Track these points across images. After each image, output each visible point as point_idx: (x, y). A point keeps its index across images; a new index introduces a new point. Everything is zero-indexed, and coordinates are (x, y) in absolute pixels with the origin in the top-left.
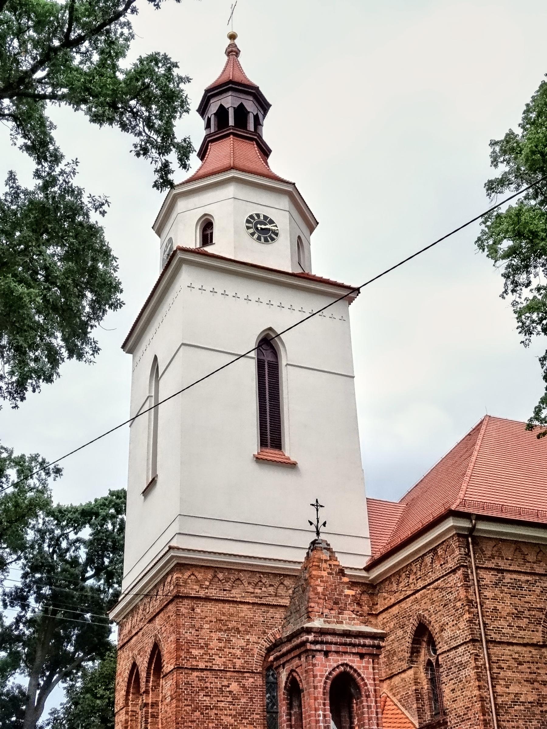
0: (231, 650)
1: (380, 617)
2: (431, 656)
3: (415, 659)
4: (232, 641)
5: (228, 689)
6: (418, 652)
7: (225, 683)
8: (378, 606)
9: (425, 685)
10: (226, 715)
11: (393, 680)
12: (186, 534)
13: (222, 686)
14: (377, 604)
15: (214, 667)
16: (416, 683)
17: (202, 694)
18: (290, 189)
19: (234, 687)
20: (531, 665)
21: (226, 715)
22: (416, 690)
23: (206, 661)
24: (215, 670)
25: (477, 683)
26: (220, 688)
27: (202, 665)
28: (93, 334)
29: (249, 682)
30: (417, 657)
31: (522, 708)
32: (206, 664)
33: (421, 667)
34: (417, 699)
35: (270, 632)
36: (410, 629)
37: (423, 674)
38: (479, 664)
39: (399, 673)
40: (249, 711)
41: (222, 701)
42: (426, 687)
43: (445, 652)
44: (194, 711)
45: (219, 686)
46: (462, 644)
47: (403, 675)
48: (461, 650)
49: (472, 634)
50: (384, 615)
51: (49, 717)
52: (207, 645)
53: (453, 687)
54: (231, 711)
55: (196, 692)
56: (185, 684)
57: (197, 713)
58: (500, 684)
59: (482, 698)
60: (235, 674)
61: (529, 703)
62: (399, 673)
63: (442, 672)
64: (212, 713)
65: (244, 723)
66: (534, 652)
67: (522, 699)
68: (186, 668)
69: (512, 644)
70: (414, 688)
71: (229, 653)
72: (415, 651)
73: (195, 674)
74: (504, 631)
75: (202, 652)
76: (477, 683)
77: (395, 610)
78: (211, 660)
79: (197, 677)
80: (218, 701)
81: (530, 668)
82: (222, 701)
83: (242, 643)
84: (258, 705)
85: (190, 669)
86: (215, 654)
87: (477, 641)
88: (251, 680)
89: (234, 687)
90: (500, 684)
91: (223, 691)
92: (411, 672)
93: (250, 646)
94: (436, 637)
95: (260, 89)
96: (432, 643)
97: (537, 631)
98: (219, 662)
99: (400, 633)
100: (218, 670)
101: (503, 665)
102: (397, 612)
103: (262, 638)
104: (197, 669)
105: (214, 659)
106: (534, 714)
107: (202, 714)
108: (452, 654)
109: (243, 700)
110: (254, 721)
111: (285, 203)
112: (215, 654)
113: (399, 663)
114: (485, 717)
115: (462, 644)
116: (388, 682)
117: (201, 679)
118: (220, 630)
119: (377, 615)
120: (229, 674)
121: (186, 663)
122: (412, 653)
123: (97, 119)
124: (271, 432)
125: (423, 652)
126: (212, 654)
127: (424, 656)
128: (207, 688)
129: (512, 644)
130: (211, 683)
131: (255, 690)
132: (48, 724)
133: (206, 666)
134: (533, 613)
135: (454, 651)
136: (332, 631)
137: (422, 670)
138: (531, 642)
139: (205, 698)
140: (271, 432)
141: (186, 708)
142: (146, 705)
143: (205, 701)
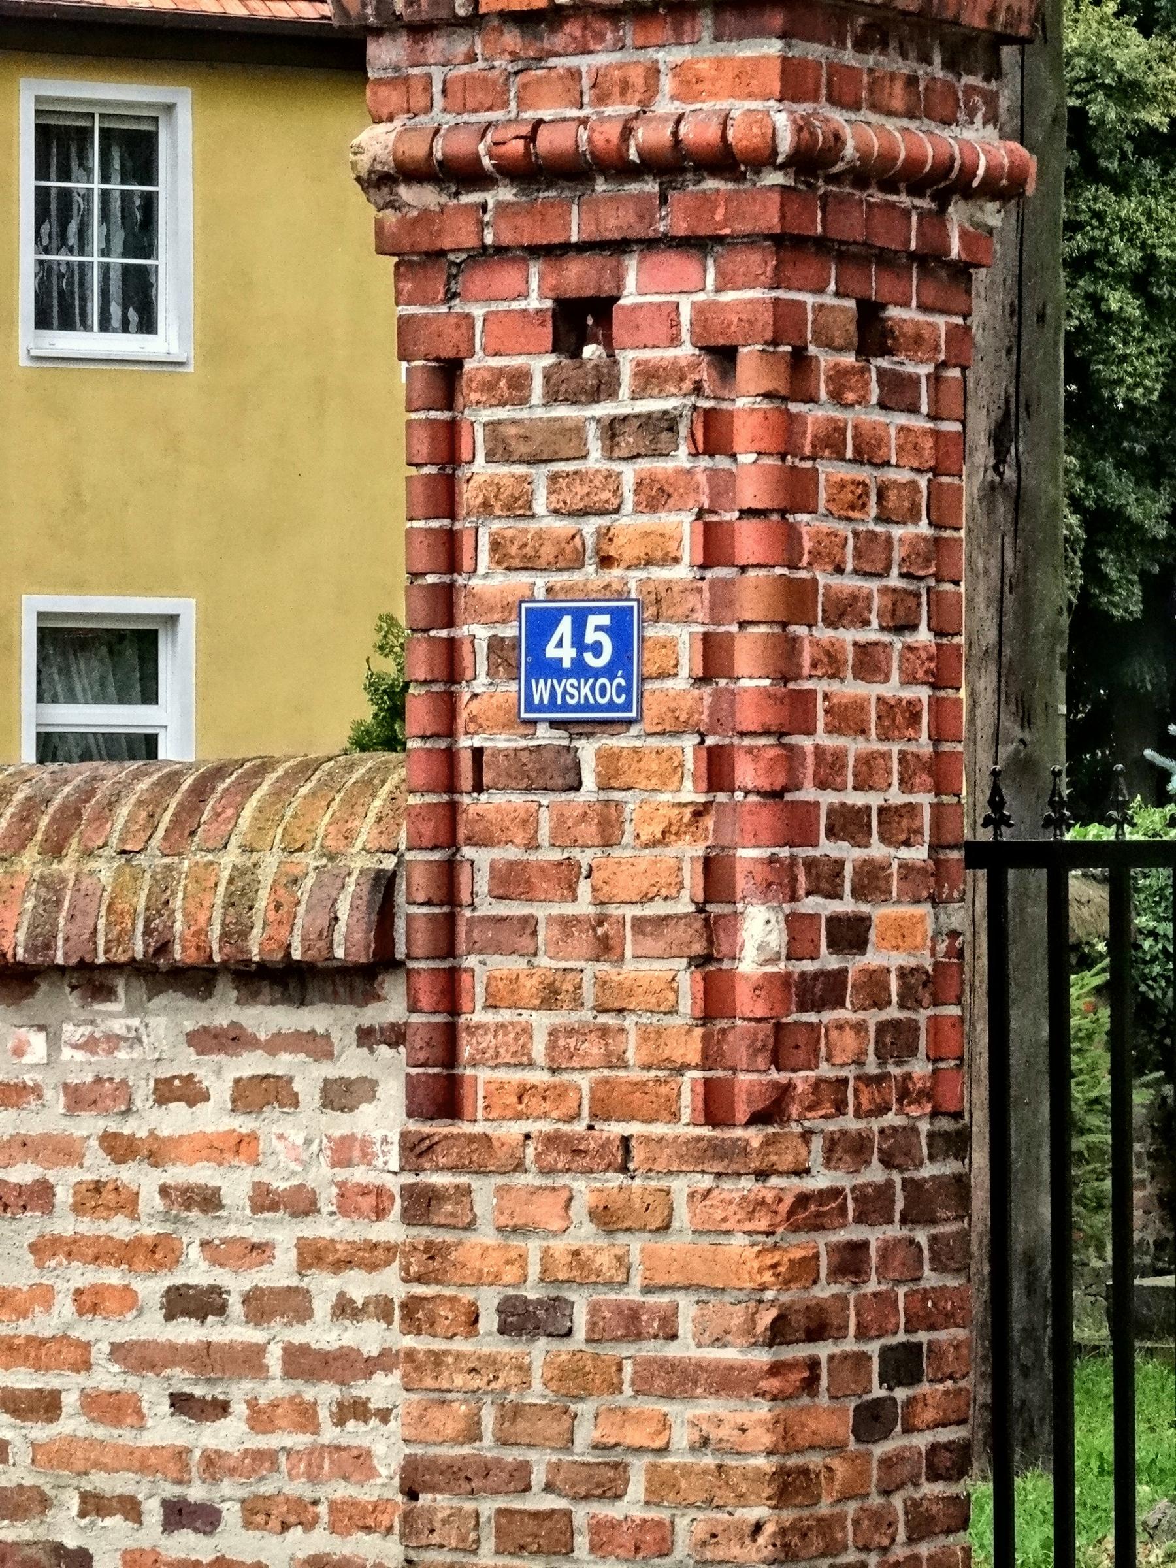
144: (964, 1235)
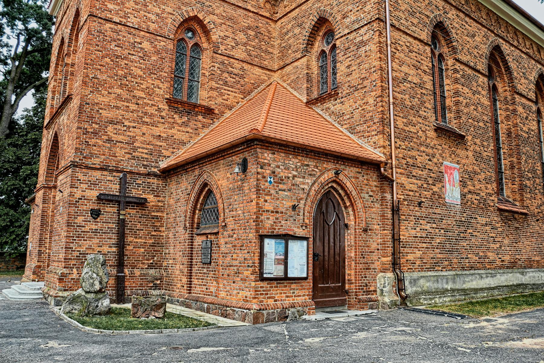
0: (147, 14)
1: (279, 23)
2: (324, 46)
3: (309, 50)
4: (148, 6)
5: (140, 46)
6: (312, 45)
7: (138, 40)
8: (278, 14)
9: (315, 70)
10: (136, 67)
11: (285, 69)
13: (135, 42)
14: (277, 13)
15: (128, 24)
16: (308, 68)
17: (114, 44)
19: (146, 45)
20: (417, 55)
21: (136, 67)
22: (307, 73)
23: (120, 17)
24: (129, 27)
25: (379, 55)
26: (132, 43)
29: (161, 44)
30: (311, 48)
31: (409, 86)
32: (121, 19)
33: (314, 58)
34: (308, 81)
35: (185, 8)
36: (309, 24)
37: (314, 62)
38: (382, 40)
39: (292, 63)
40: (158, 68)
41: (133, 55)
42: (316, 72)
43: (345, 35)
44: (103, 57)
45: (132, 41)
46: (366, 25)
47: (296, 64)
48: (363, 31)
49: (379, 14)
50: (283, 20)
51: (23, 113)
53: (350, 63)
54: (141, 65)
55: (108, 42)
56: (98, 32)
57: (107, 60)
58: (395, 62)
59: (382, 68)
60: (148, 35)
61: (414, 83)
62: (292, 63)
63: (338, 53)
64: (123, 63)
65: (152, 77)
66: (421, 47)
67: (409, 79)
68: (100, 18)
69: (407, 34)
70: (306, 72)
71: (144, 16)
72: (310, 43)
73: (108, 25)
74: (402, 21)
75: (117, 8)
76: (379, 55)
77: (294, 14)
78: (126, 16)
79: (110, 28)
80: (129, 54)
81: (416, 57)
82: (133, 55)
83: (158, 11)
84: (168, 66)
85: (104, 20)
86: (130, 13)
87: (382, 21)
89: (146, 45)
90: (395, 62)
91: (135, 46)
92: (305, 60)
93: (164, 15)
94: (336, 27)
96: (330, 34)
97: (424, 31)
98: (133, 21)
99: (297, 31)
100: (132, 27)
101: (399, 48)
102: (296, 14)
103: (177, 12)
104: (111, 21)
105: (129, 17)
106: (417, 94)
107: (112, 61)
108: (351, 37)
110: (162, 78)
112: (130, 13)
113: (293, 55)
114: (383, 84)
115: (366, 25)
116: (280, 71)
119: (276, 21)
120: (142, 33)
121: (100, 13)
122: (308, 44)
125: (317, 44)
126: (128, 12)
127: (319, 45)
128: (119, 40)
129: (407, 34)
130: (124, 37)
131: (154, 188)
132: (22, 119)
133: (120, 21)
134: (423, 17)
135: (355, 33)
137: (314, 59)
138: (419, 37)
139: (116, 48)
141: (96, 52)
142: (67, 65)
143: (117, 50)
144: (446, 123)
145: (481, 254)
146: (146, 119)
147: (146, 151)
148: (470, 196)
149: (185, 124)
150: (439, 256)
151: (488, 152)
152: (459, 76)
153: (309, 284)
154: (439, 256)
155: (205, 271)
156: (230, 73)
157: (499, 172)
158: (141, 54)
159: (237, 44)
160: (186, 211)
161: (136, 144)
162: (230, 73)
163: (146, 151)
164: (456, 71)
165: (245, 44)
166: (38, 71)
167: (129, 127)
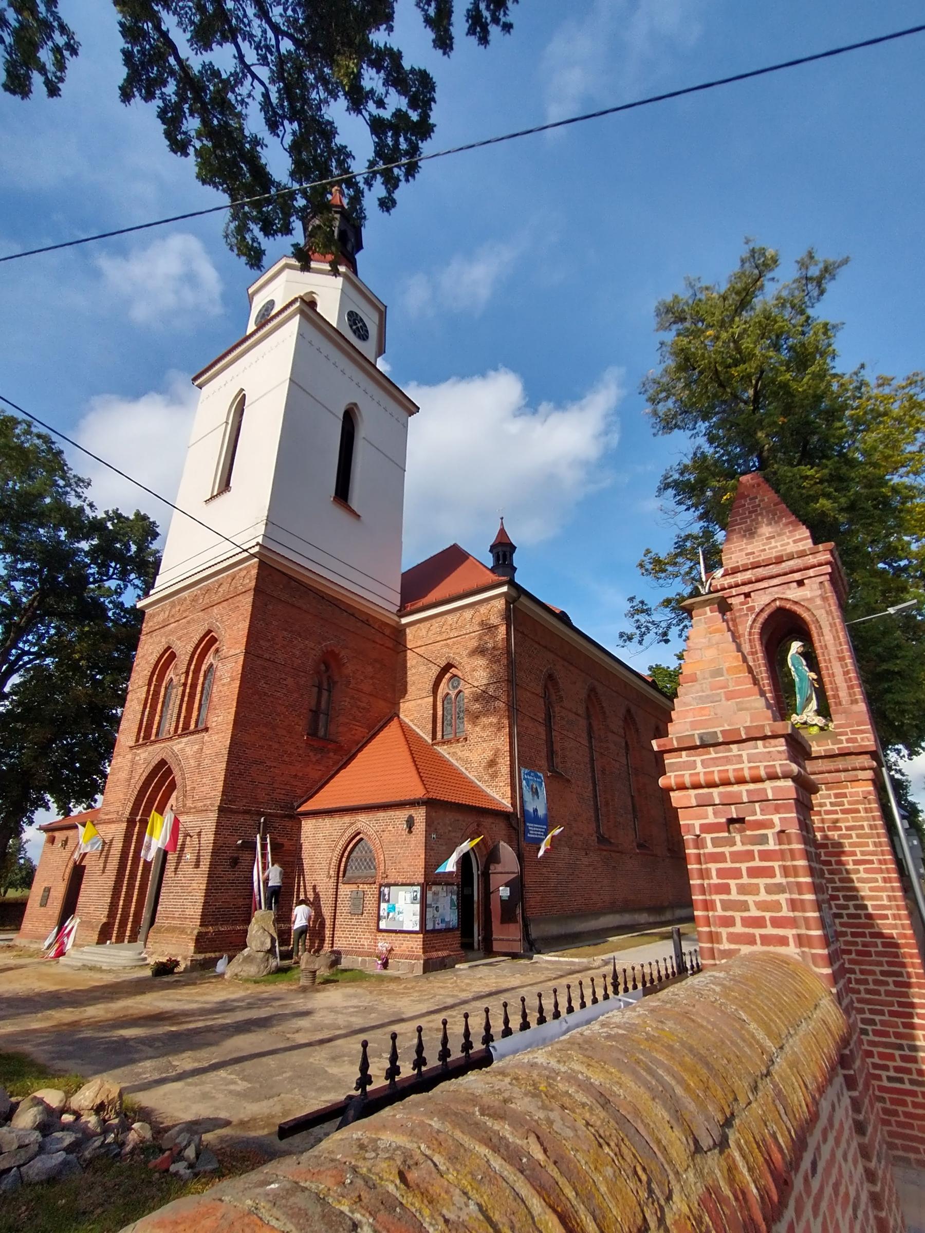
7: (283, 676)
12: (594, 115)
18: (383, 309)
27: (267, 656)
28: (671, 363)
52: (273, 639)
57: (256, 697)
73: (259, 662)
75: (268, 644)
88: (304, 679)
89: (290, 681)
95: (121, 82)
109: (296, 695)
111: (375, 317)
117: (264, 668)
118: (286, 630)
123: (468, 10)
124: (342, 493)
136: (364, 618)
140: (342, 493)
145: (586, 896)
146: (286, 758)
147: (283, 792)
148: (575, 837)
149: (318, 762)
150: (554, 899)
151: (588, 794)
152: (564, 723)
153: (458, 933)
154: (554, 899)
155: (354, 922)
156: (358, 707)
157: (597, 810)
158: (284, 691)
159: (365, 677)
160: (331, 859)
161: (275, 785)
162: (358, 707)
163: (283, 792)
164: (562, 718)
165: (372, 678)
166: (114, 682)
167: (271, 767)
